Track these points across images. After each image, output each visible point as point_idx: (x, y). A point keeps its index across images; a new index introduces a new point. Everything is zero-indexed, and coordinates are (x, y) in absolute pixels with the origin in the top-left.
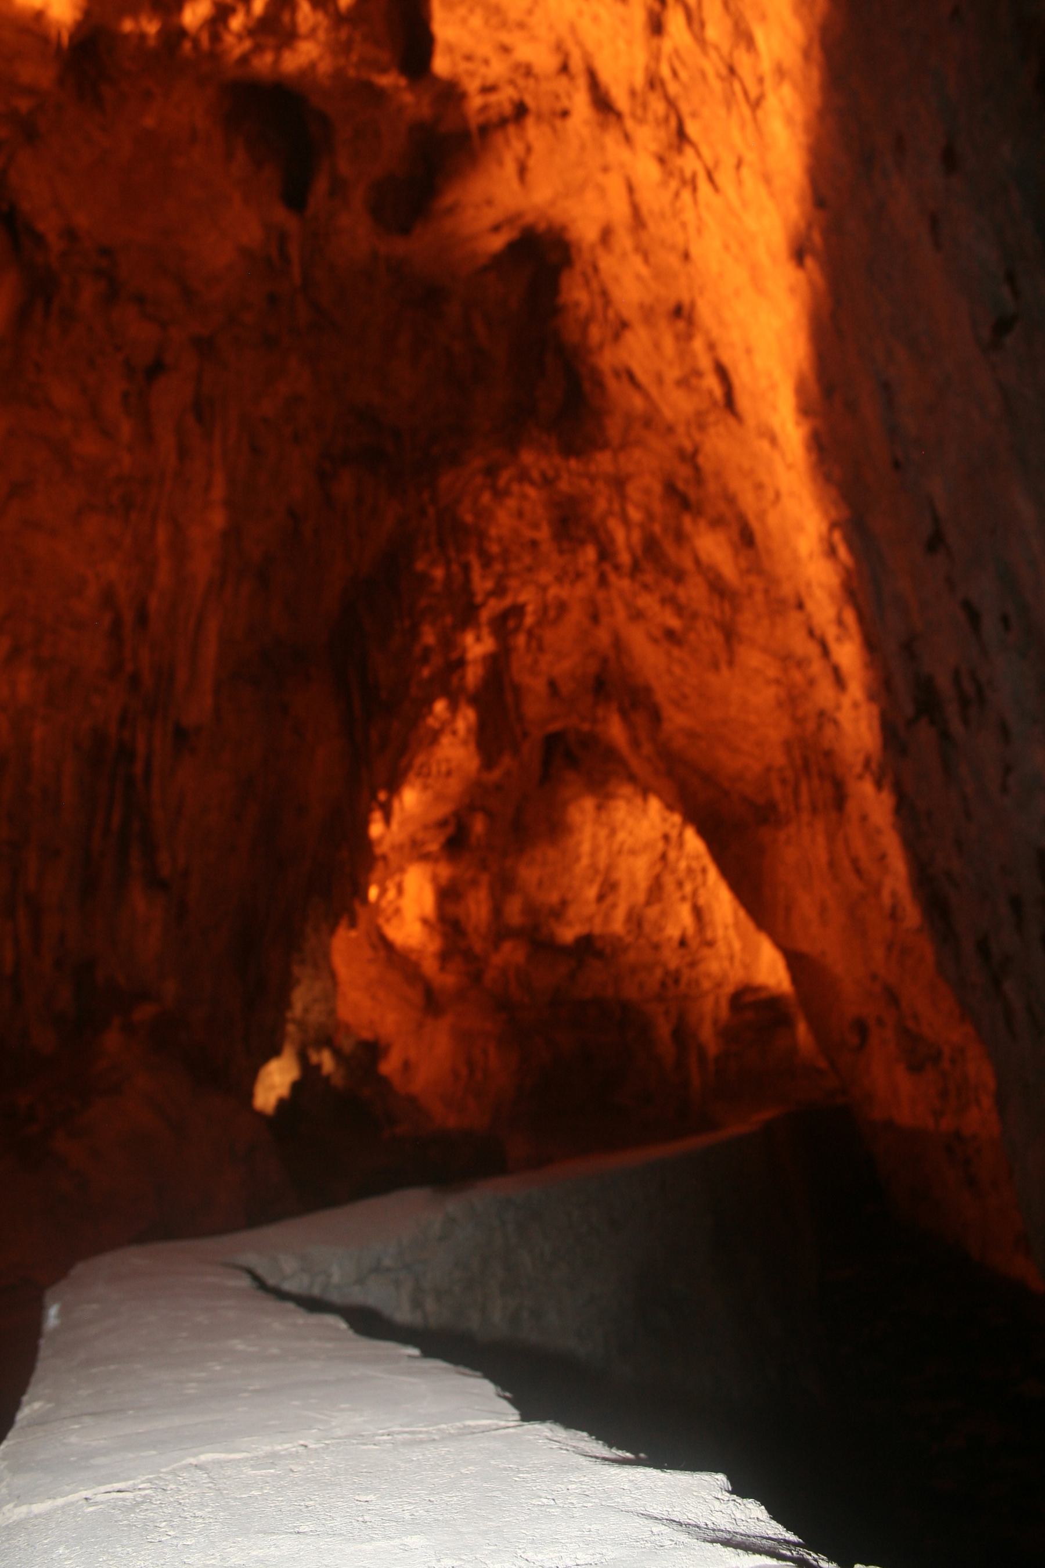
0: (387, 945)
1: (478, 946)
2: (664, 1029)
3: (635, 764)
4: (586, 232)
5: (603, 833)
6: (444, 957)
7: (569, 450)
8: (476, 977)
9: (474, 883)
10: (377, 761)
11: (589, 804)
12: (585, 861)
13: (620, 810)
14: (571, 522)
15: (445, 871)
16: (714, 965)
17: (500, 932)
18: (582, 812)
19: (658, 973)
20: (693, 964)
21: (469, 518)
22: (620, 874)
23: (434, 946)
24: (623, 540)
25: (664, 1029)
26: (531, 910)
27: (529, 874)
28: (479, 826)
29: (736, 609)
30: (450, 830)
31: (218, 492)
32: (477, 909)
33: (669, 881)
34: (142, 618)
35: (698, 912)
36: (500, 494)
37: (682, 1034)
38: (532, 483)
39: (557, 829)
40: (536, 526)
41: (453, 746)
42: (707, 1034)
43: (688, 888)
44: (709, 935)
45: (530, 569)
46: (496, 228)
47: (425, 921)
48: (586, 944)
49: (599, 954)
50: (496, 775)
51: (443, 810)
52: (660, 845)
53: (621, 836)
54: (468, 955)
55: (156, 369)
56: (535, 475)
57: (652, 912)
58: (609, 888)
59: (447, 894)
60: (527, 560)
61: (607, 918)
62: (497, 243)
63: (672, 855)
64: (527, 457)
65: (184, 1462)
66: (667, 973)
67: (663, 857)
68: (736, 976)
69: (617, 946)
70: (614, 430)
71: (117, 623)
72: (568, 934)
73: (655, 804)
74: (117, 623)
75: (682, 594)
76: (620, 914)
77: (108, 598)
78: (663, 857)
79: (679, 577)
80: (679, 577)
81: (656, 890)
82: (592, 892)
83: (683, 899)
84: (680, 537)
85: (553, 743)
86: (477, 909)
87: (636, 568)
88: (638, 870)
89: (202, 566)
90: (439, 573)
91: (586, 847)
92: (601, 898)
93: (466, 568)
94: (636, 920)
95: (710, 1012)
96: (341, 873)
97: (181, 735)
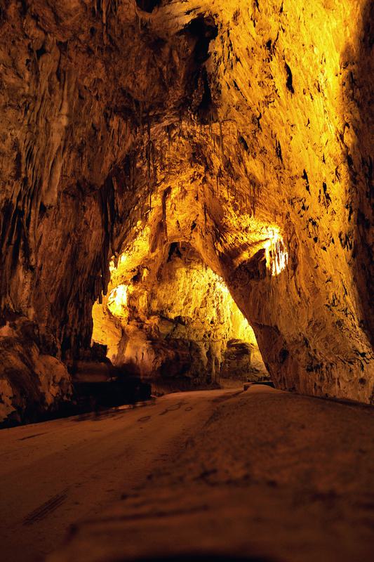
0: (110, 313)
1: (142, 317)
2: (204, 352)
3: (204, 256)
4: (227, 17)
5: (188, 281)
6: (129, 319)
7: (203, 122)
8: (141, 328)
9: (142, 294)
10: (113, 243)
11: (184, 270)
12: (181, 290)
13: (194, 273)
14: (198, 155)
15: (131, 289)
16: (222, 330)
17: (150, 313)
18: (181, 272)
19: (203, 332)
20: (215, 330)
21: (158, 148)
22: (193, 296)
23: (126, 315)
24: (217, 162)
25: (204, 352)
26: (160, 305)
27: (161, 293)
28: (145, 273)
29: (259, 191)
30: (135, 273)
31: (65, 110)
32: (142, 303)
33: (209, 300)
34: (30, 156)
35: (218, 311)
36: (171, 140)
37: (209, 354)
38: (184, 137)
39: (172, 278)
40: (183, 155)
41: (141, 245)
42: (219, 355)
43: (216, 304)
44: (222, 321)
45: (178, 172)
46: (188, 13)
47: (123, 306)
48: (179, 320)
49: (184, 324)
50: (154, 254)
51: (134, 265)
52: (208, 287)
53: (194, 283)
54: (138, 319)
55: (42, 52)
56: (185, 133)
57: (203, 311)
58: (188, 300)
59: (131, 297)
60: (178, 168)
61: (187, 312)
62: (187, 19)
63: (211, 291)
64: (184, 125)
65: (54, 153)
66: (206, 332)
67: (208, 291)
68: (230, 336)
69: (190, 322)
70: (221, 113)
71: (19, 156)
72: (172, 316)
73: (210, 271)
74: (19, 156)
75: (237, 186)
76: (192, 310)
77: (15, 146)
78: (208, 291)
79: (237, 178)
80: (237, 178)
81: (204, 303)
82: (182, 302)
83: (214, 307)
84: (241, 160)
85: (174, 247)
86: (142, 303)
87: (220, 174)
88: (198, 296)
89: (57, 139)
90: (145, 169)
91: (181, 285)
92: (185, 304)
93: (155, 169)
94: (196, 313)
95: (220, 348)
96: (98, 285)
97: (43, 210)
